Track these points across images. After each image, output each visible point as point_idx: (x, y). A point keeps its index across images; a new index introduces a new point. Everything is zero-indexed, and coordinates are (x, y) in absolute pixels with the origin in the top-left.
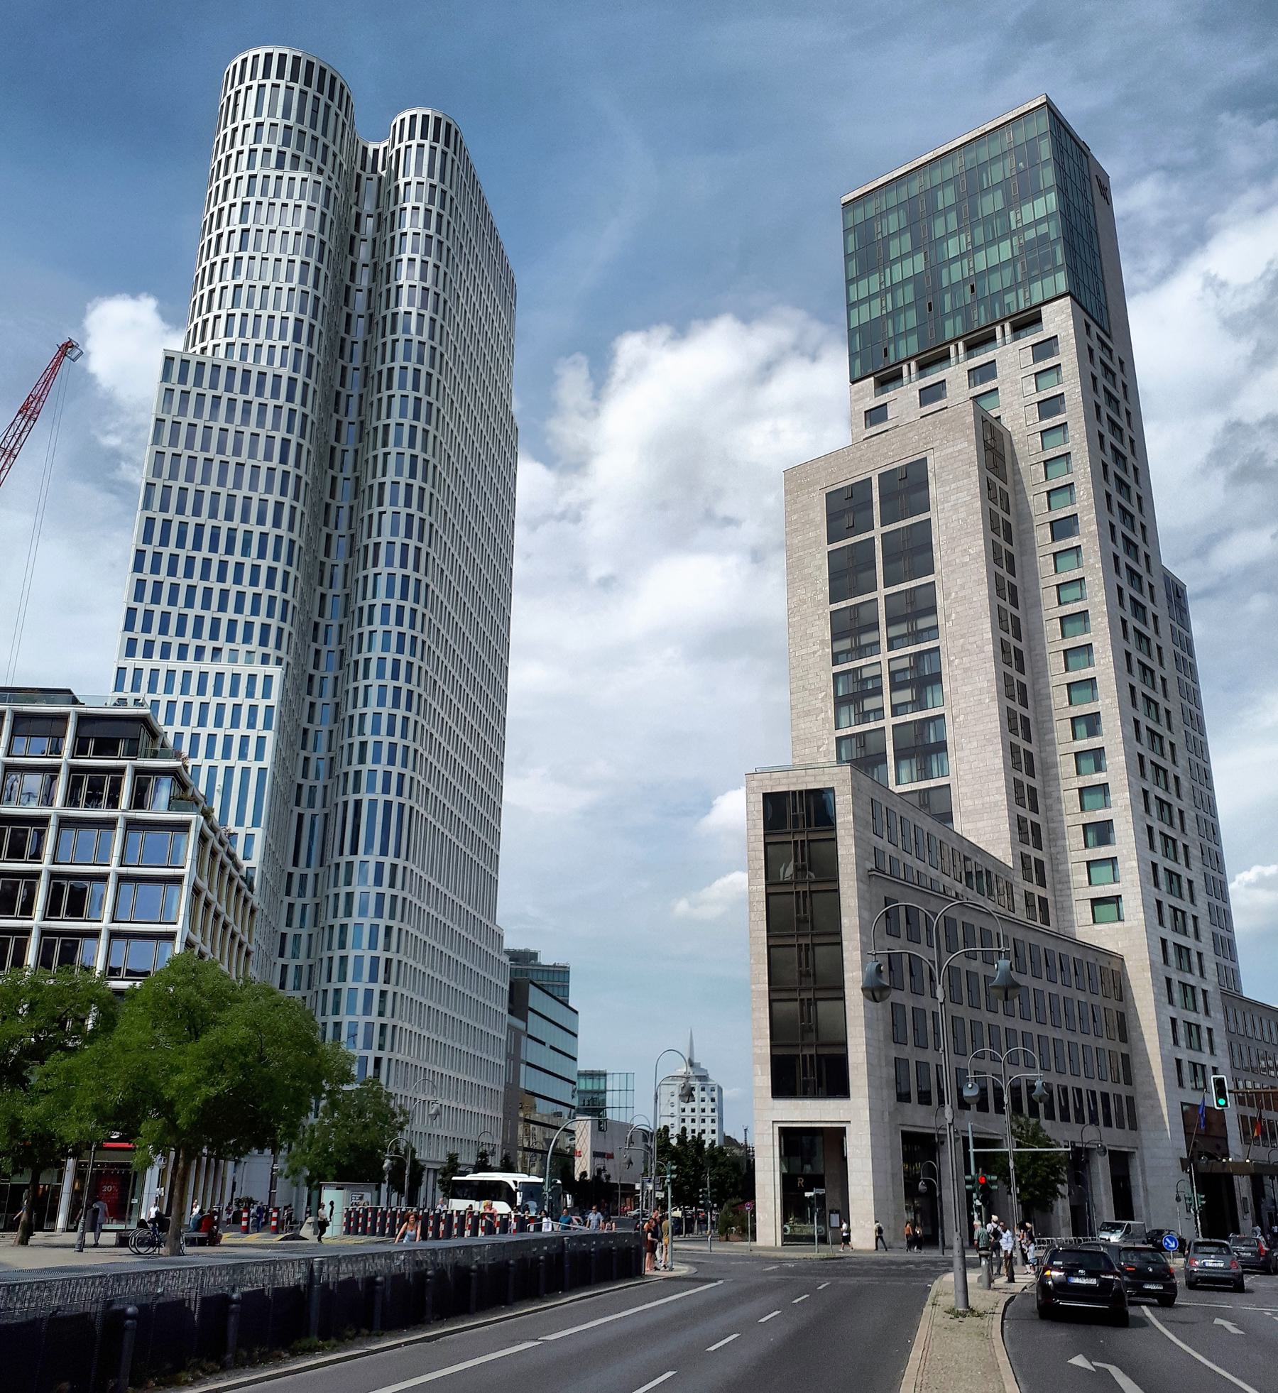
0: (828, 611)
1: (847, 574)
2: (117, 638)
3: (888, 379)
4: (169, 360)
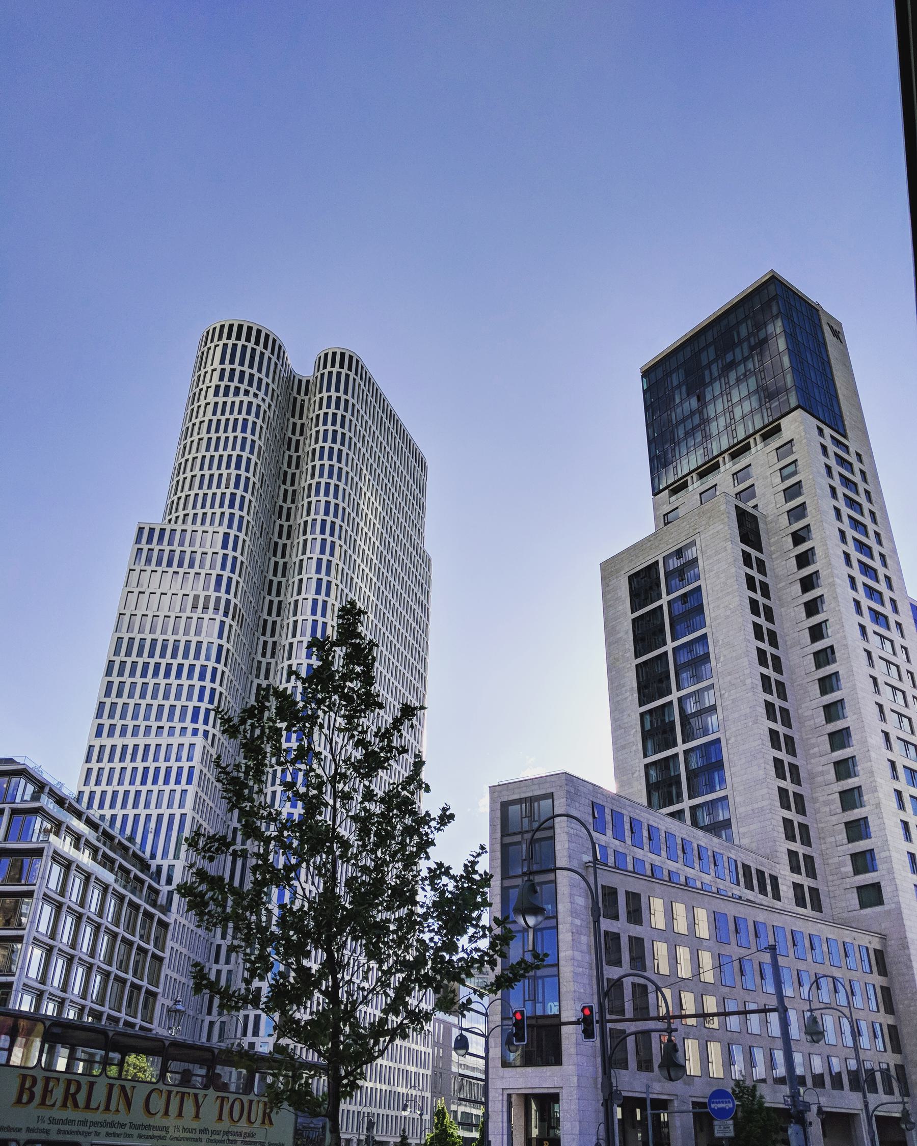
0: (634, 665)
1: (646, 633)
2: (88, 723)
4: (141, 529)
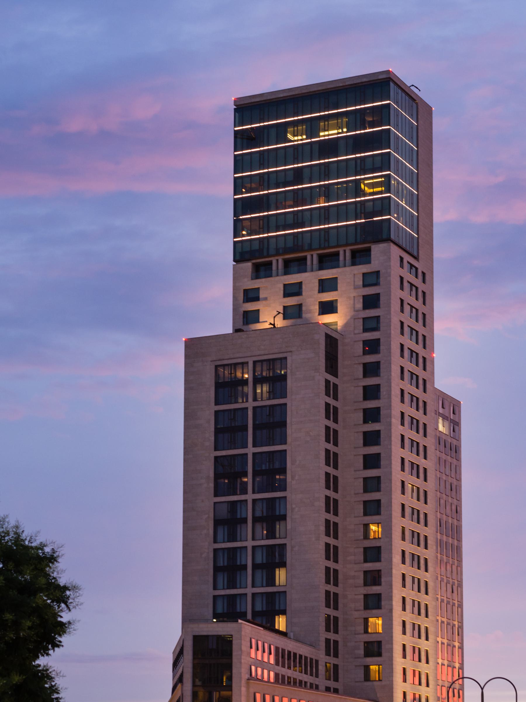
3: (262, 270)
